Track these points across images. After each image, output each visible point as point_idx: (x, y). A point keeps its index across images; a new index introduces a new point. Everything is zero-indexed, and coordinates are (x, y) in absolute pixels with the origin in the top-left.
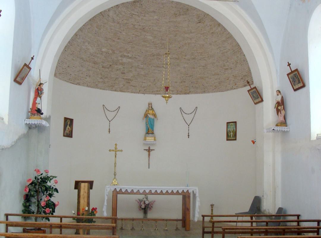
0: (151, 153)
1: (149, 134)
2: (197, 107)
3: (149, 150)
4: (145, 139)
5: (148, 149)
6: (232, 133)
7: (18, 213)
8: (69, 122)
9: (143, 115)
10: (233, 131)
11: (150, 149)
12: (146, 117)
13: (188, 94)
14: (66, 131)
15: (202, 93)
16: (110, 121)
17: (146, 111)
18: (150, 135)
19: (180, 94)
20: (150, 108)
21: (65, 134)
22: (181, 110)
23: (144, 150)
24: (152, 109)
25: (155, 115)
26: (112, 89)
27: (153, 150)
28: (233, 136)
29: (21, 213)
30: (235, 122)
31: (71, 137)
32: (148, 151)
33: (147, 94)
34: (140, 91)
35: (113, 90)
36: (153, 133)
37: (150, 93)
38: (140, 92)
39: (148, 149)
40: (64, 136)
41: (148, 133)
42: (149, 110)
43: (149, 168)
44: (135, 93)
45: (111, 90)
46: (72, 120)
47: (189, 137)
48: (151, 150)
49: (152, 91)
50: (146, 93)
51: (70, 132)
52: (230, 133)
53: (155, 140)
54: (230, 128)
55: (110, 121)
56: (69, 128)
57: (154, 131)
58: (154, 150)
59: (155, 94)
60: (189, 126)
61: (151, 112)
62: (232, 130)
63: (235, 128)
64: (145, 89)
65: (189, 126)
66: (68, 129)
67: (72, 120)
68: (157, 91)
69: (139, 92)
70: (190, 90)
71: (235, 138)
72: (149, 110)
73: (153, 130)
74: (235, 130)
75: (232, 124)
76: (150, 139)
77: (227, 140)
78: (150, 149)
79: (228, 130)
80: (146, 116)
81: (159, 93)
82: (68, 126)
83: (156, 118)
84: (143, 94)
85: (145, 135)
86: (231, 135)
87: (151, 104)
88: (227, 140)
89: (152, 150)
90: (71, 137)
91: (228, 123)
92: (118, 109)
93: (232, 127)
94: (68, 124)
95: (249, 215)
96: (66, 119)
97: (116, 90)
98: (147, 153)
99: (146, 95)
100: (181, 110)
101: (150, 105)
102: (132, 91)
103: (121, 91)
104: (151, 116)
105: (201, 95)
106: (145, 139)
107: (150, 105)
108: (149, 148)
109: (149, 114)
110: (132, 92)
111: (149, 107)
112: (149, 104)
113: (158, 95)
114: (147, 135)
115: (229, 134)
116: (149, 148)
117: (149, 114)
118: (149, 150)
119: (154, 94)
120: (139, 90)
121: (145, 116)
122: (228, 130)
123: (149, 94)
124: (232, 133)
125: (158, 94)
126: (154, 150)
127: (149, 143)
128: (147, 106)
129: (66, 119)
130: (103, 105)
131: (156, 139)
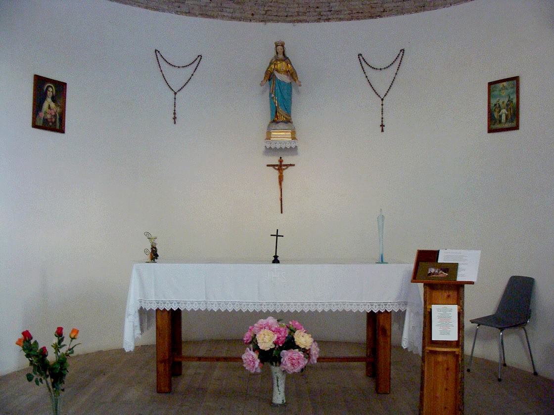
0: (286, 173)
1: (278, 123)
2: (403, 50)
3: (280, 167)
4: (268, 138)
5: (278, 163)
6: (504, 111)
7: (475, 352)
8: (50, 89)
9: (263, 75)
10: (507, 105)
11: (283, 163)
12: (269, 80)
13: (380, 16)
14: (42, 115)
15: (416, 12)
16: (175, 93)
17: (271, 64)
18: (281, 126)
19: (358, 19)
20: (281, 56)
21: (40, 122)
22: (362, 60)
23: (268, 166)
24: (286, 59)
25: (292, 74)
26: (178, 9)
27: (291, 165)
28: (510, 116)
29: (184, 363)
30: (516, 79)
31: (62, 130)
32: (277, 168)
33: (272, 20)
34: (253, 15)
35: (182, 13)
36: (288, 121)
37: (277, 19)
38: (255, 16)
39: (278, 163)
40: (35, 126)
41: (275, 121)
42: (277, 60)
43: (282, 213)
44: (240, 19)
45: (177, 12)
46: (61, 87)
47: (382, 131)
48: (284, 165)
49: (286, 14)
50: (269, 21)
51: (55, 116)
52: (497, 110)
53: (294, 138)
54: (500, 96)
55: (175, 93)
56: (53, 105)
57: (292, 116)
58: (294, 165)
59: (294, 22)
60: (382, 100)
61: (281, 66)
62: (506, 102)
63: (514, 97)
64: (266, 9)
65: (382, 100)
66: (49, 108)
67: (61, 87)
68: (298, 14)
69: (252, 18)
70: (386, 5)
71: (514, 124)
72: (277, 60)
73: (289, 114)
74: (515, 101)
75: (505, 84)
76: (281, 136)
77: (490, 131)
78: (283, 163)
79: (493, 101)
80: (270, 76)
81: (304, 18)
82: (48, 102)
83: (295, 80)
84: (262, 21)
85: (269, 126)
86: (501, 116)
87: (283, 45)
88: (490, 131)
89: (288, 166)
90: (62, 130)
91: (490, 84)
92: (197, 61)
93: (504, 93)
94: (50, 94)
95: (460, 340)
96: (40, 82)
97: (188, 13)
98: (276, 173)
99: (270, 24)
100: (362, 60)
101: (280, 47)
102: (234, 16)
103: (204, 15)
104: (282, 77)
105: (414, 15)
106: (268, 138)
107: (280, 47)
108: (281, 161)
109: (277, 70)
110: (233, 18)
111: (277, 53)
112: (277, 46)
113: (300, 24)
114: (274, 126)
115: (496, 115)
116: (281, 161)
117: (277, 70)
118: (280, 167)
119: (290, 22)
120: (250, 12)
121: (268, 76)
122: (493, 101)
123: (278, 21)
124: (504, 111)
125: (300, 21)
126: (294, 165)
127: (278, 146)
128: (274, 53)
129: (40, 82)
130: (156, 50)
131: (297, 136)
